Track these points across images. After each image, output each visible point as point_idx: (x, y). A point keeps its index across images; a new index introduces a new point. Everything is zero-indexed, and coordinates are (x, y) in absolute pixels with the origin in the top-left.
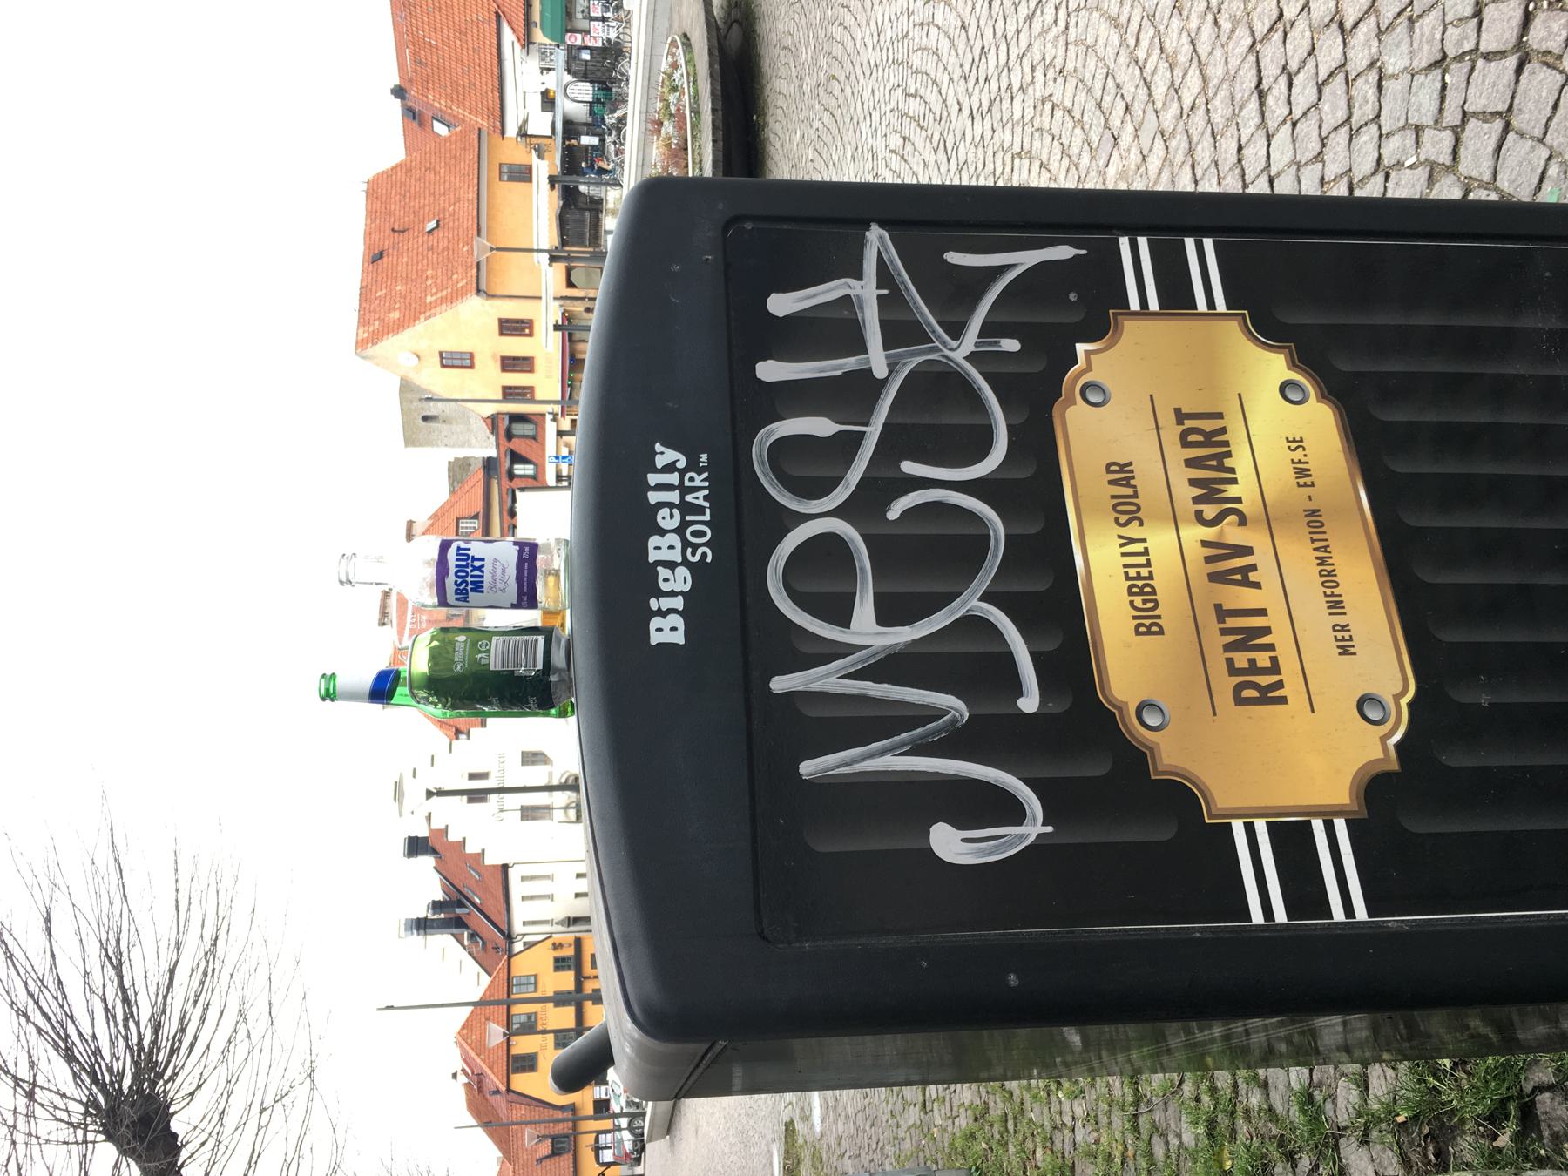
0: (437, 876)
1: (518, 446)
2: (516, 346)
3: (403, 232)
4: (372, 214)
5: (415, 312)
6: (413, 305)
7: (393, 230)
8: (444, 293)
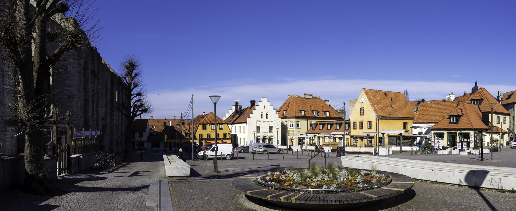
0: (246, 108)
1: (343, 126)
2: (365, 125)
4: (395, 93)
5: (372, 102)
7: (392, 98)
8: (377, 109)
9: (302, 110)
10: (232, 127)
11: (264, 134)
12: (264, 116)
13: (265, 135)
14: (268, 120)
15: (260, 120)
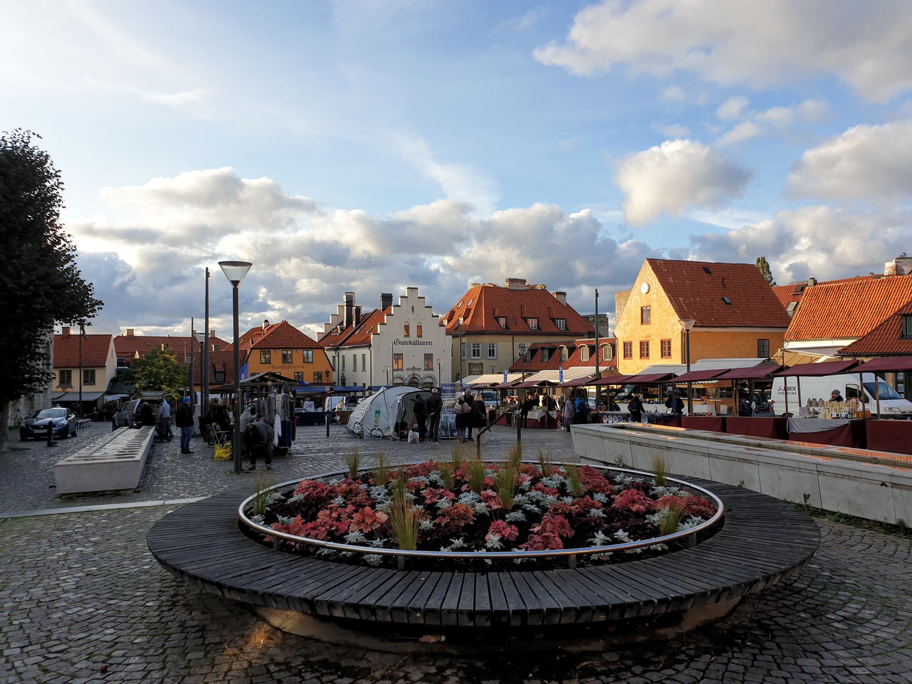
2: (655, 349)
3: (723, 284)
6: (677, 290)
7: (724, 279)
9: (502, 317)
10: (337, 357)
11: (412, 372)
12: (413, 331)
13: (414, 375)
14: (421, 340)
15: (402, 339)
